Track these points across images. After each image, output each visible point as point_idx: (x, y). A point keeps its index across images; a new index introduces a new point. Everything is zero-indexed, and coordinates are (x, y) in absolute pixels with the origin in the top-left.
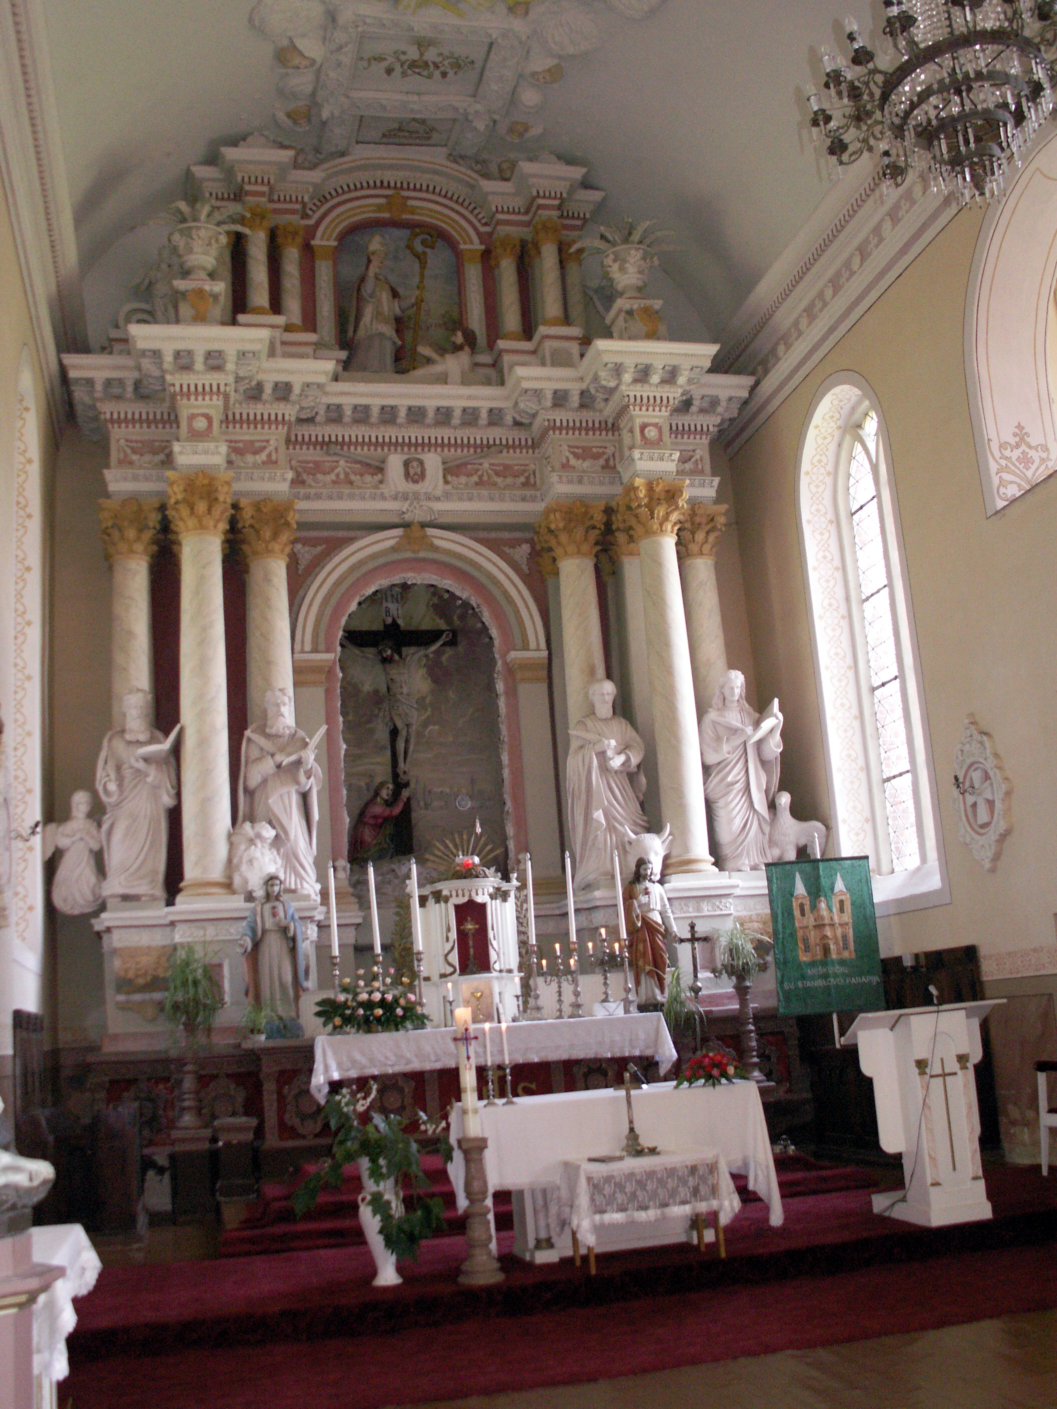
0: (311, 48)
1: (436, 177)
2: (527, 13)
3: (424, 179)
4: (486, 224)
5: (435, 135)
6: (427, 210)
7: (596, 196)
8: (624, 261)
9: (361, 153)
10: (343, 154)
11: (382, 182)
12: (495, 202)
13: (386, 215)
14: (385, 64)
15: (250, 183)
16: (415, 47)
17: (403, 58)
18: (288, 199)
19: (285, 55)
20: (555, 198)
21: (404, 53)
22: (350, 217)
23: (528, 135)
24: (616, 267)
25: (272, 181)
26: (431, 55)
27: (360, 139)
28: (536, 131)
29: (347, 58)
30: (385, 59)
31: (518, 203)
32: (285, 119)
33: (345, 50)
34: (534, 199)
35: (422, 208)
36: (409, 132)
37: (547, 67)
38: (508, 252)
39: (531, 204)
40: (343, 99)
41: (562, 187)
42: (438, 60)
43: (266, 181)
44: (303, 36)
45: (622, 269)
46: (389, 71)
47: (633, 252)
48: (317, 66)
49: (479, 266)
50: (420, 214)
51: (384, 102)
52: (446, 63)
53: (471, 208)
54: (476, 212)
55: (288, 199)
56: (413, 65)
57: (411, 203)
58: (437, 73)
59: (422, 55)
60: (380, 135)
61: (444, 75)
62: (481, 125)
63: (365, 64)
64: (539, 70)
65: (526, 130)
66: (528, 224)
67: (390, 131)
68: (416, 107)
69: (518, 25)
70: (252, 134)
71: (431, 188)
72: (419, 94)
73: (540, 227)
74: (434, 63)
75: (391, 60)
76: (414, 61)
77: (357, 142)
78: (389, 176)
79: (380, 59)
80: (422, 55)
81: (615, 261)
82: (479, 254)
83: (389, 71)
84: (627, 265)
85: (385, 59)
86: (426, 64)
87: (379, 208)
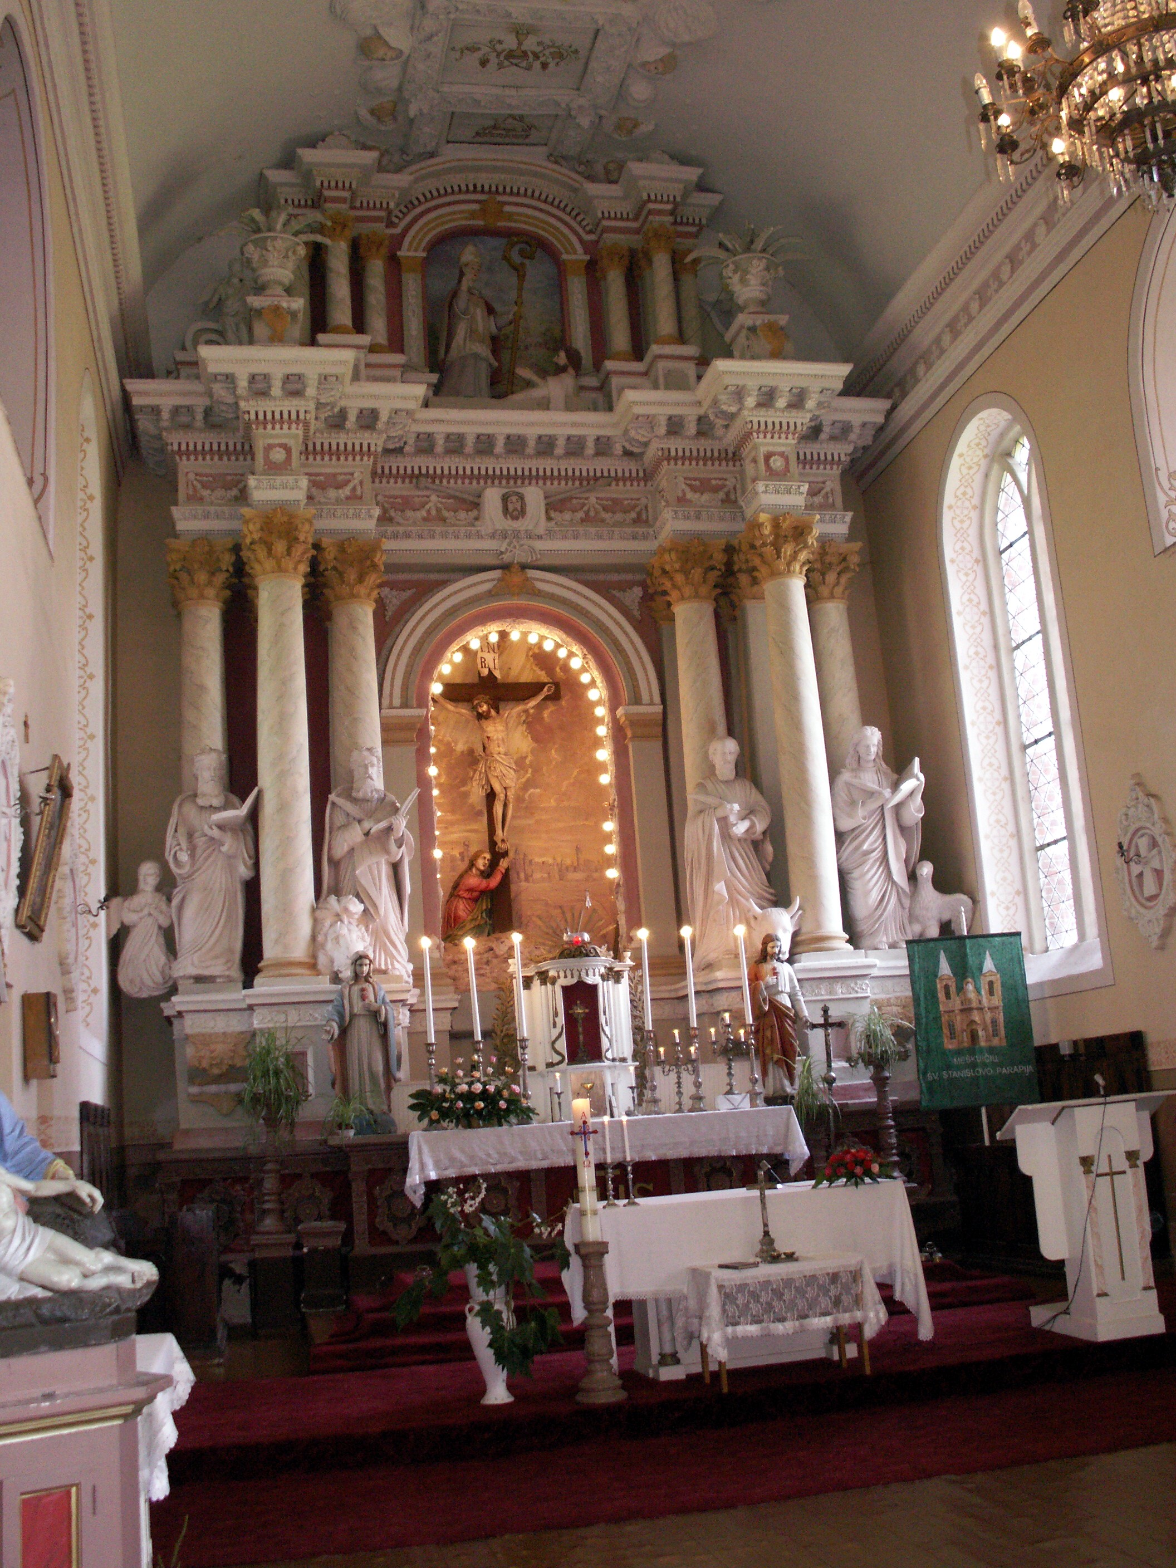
3: (520, 182)
4: (590, 232)
6: (525, 216)
8: (746, 272)
9: (451, 154)
12: (601, 207)
14: (478, 55)
17: (499, 48)
19: (369, 46)
20: (668, 202)
21: (500, 42)
23: (637, 132)
24: (736, 278)
26: (530, 44)
28: (646, 128)
30: (479, 49)
31: (626, 208)
32: (368, 116)
33: (435, 39)
35: (518, 214)
36: (505, 130)
37: (659, 57)
42: (538, 49)
45: (743, 281)
46: (484, 63)
49: (583, 279)
54: (579, 219)
56: (510, 55)
58: (537, 65)
61: (545, 66)
65: (635, 126)
66: (637, 231)
75: (485, 50)
78: (484, 179)
79: (473, 49)
80: (520, 44)
81: (735, 272)
83: (484, 63)
87: (473, 215)
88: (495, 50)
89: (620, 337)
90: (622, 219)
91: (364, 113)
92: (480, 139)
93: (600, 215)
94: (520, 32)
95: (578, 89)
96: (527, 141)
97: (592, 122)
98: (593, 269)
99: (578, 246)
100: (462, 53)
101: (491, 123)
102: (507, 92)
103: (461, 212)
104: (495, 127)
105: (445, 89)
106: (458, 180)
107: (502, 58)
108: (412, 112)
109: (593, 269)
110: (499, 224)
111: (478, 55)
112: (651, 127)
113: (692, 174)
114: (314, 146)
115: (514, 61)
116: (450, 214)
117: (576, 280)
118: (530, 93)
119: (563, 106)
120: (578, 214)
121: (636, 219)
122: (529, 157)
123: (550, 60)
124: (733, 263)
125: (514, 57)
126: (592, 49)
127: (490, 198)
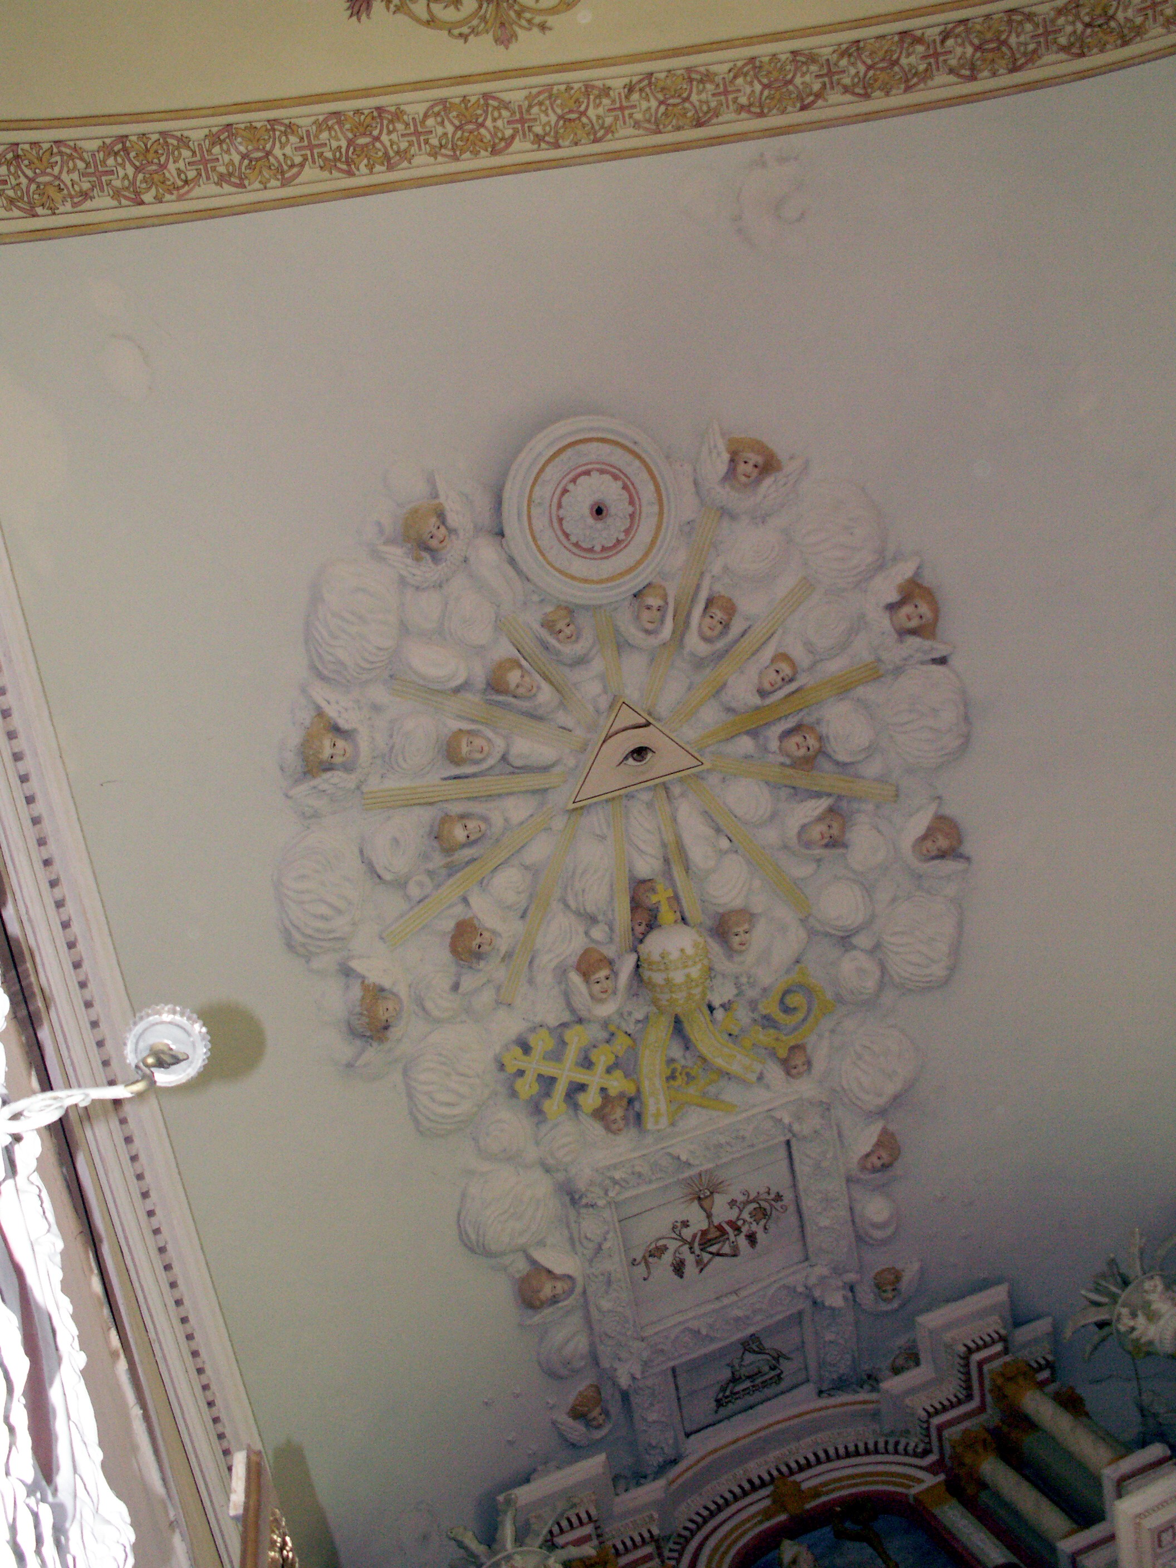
0: (559, 1260)
1: (820, 1436)
2: (809, 1063)
3: (803, 1449)
4: (926, 1452)
5: (785, 1366)
6: (833, 1480)
7: (1042, 1326)
8: (1146, 1305)
9: (697, 1447)
10: (674, 1462)
11: (750, 1481)
12: (920, 1403)
13: (782, 1517)
14: (668, 1258)
15: (562, 1531)
16: (696, 1204)
17: (687, 1233)
18: (629, 1543)
19: (533, 1291)
20: (994, 1342)
21: (685, 1224)
22: (729, 1547)
23: (903, 1285)
24: (1141, 1320)
25: (593, 1512)
26: (722, 1212)
27: (688, 1430)
28: (910, 1271)
29: (615, 1264)
30: (665, 1248)
31: (950, 1389)
32: (570, 1421)
33: (606, 1245)
34: (966, 1358)
35: (824, 1484)
36: (749, 1372)
37: (874, 1139)
38: (981, 1450)
39: (967, 1365)
40: (636, 1344)
41: (993, 1324)
42: (733, 1214)
43: (584, 1516)
44: (541, 1243)
45: (1152, 1316)
46: (679, 1269)
47: (1147, 1285)
48: (579, 1289)
49: (954, 1502)
50: (827, 1493)
51: (694, 1325)
52: (746, 1215)
53: (891, 1448)
54: (901, 1448)
55: (629, 1543)
56: (706, 1240)
57: (805, 1486)
58: (742, 1242)
59: (709, 1216)
60: (713, 1405)
61: (752, 1238)
62: (835, 1299)
63: (642, 1269)
64: (868, 1149)
65: (898, 1278)
66: (982, 1408)
67: (723, 1389)
68: (738, 1313)
69: (806, 1088)
70: (535, 1470)
71: (822, 1455)
72: (735, 1292)
73: (999, 1381)
74: (730, 1223)
75: (673, 1245)
76: (704, 1233)
77: (688, 1435)
78: (757, 1468)
79: (658, 1251)
80: (709, 1216)
81: (1134, 1315)
82: (943, 1488)
83: (679, 1269)
84: (1154, 1307)
85: (665, 1248)
86: (720, 1228)
87: (767, 1514)
88: (685, 1241)
89: (1050, 1519)
90: (952, 1406)
91: (563, 1418)
92: (723, 1412)
93: (924, 1414)
94: (702, 1194)
95: (807, 1259)
96: (788, 1196)
97: (845, 1298)
98: (963, 1486)
99: (920, 1474)
100: (647, 1263)
101: (727, 1374)
102: (726, 1301)
103: (752, 1517)
104: (735, 1380)
105: (649, 1331)
106: (725, 1484)
107: (698, 1251)
108: (624, 1382)
109: (963, 1486)
110: (808, 1506)
111: (668, 1258)
112: (916, 1266)
113: (999, 1294)
114: (527, 1480)
115: (714, 1249)
116: (736, 1527)
117: (946, 1508)
118: (750, 1289)
119: (800, 1289)
120: (897, 1443)
121: (969, 1397)
122: (796, 1404)
123: (754, 1227)
124: (1123, 1306)
125: (711, 1242)
126: (794, 1186)
127: (779, 1482)
